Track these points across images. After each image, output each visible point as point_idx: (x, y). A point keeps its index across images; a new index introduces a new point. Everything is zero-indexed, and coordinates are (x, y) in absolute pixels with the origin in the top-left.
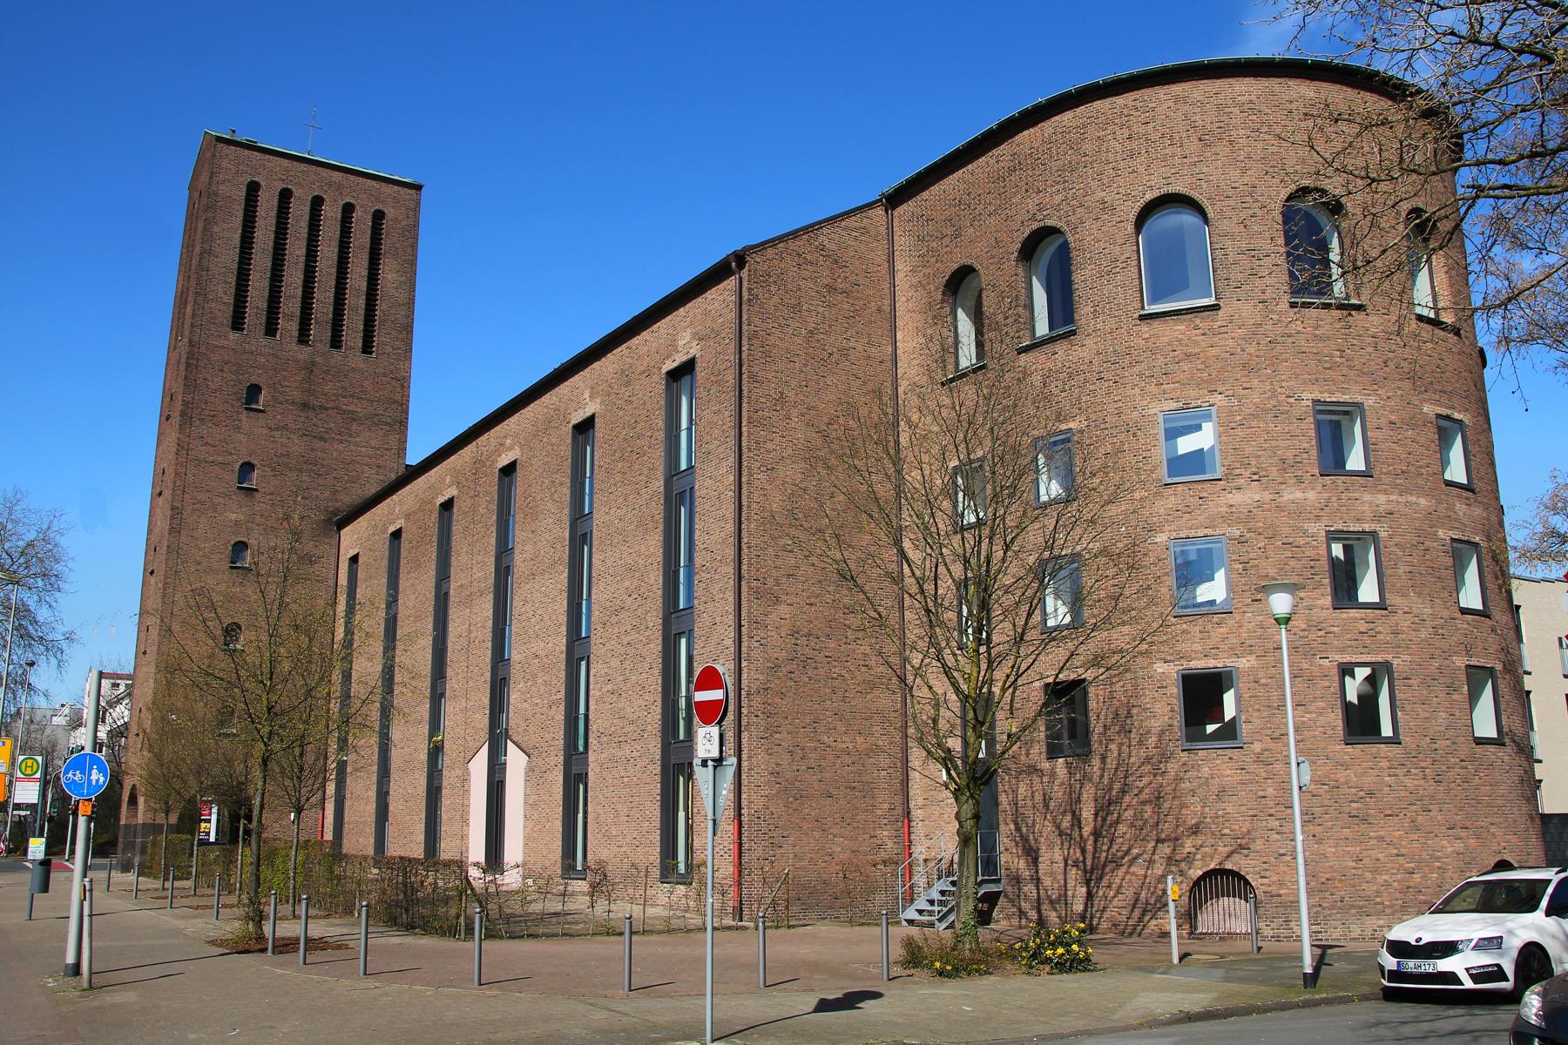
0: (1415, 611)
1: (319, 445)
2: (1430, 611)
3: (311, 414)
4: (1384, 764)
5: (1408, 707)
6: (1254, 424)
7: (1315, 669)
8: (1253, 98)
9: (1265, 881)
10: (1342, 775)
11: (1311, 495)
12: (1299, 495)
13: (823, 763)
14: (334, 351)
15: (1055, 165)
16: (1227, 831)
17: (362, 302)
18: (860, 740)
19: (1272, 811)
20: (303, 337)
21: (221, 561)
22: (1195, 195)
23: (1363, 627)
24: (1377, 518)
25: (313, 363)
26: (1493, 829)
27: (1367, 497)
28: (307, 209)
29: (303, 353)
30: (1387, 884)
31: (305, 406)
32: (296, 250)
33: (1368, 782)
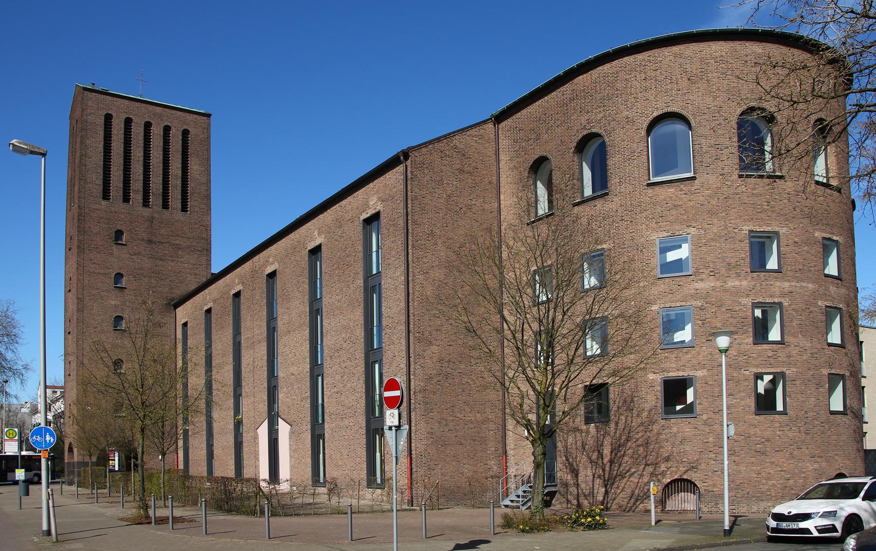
0: (801, 345)
1: (160, 263)
2: (809, 345)
3: (154, 246)
4: (777, 425)
5: (793, 396)
8: (723, 53)
10: (752, 431)
12: (737, 283)
14: (165, 211)
15: (598, 96)
17: (179, 182)
18: (478, 415)
20: (146, 203)
21: (108, 326)
22: (684, 113)
23: (770, 354)
24: (783, 295)
25: (153, 218)
27: (778, 284)
28: (142, 129)
29: (146, 212)
30: (774, 485)
31: (150, 242)
32: (137, 153)
33: (768, 434)
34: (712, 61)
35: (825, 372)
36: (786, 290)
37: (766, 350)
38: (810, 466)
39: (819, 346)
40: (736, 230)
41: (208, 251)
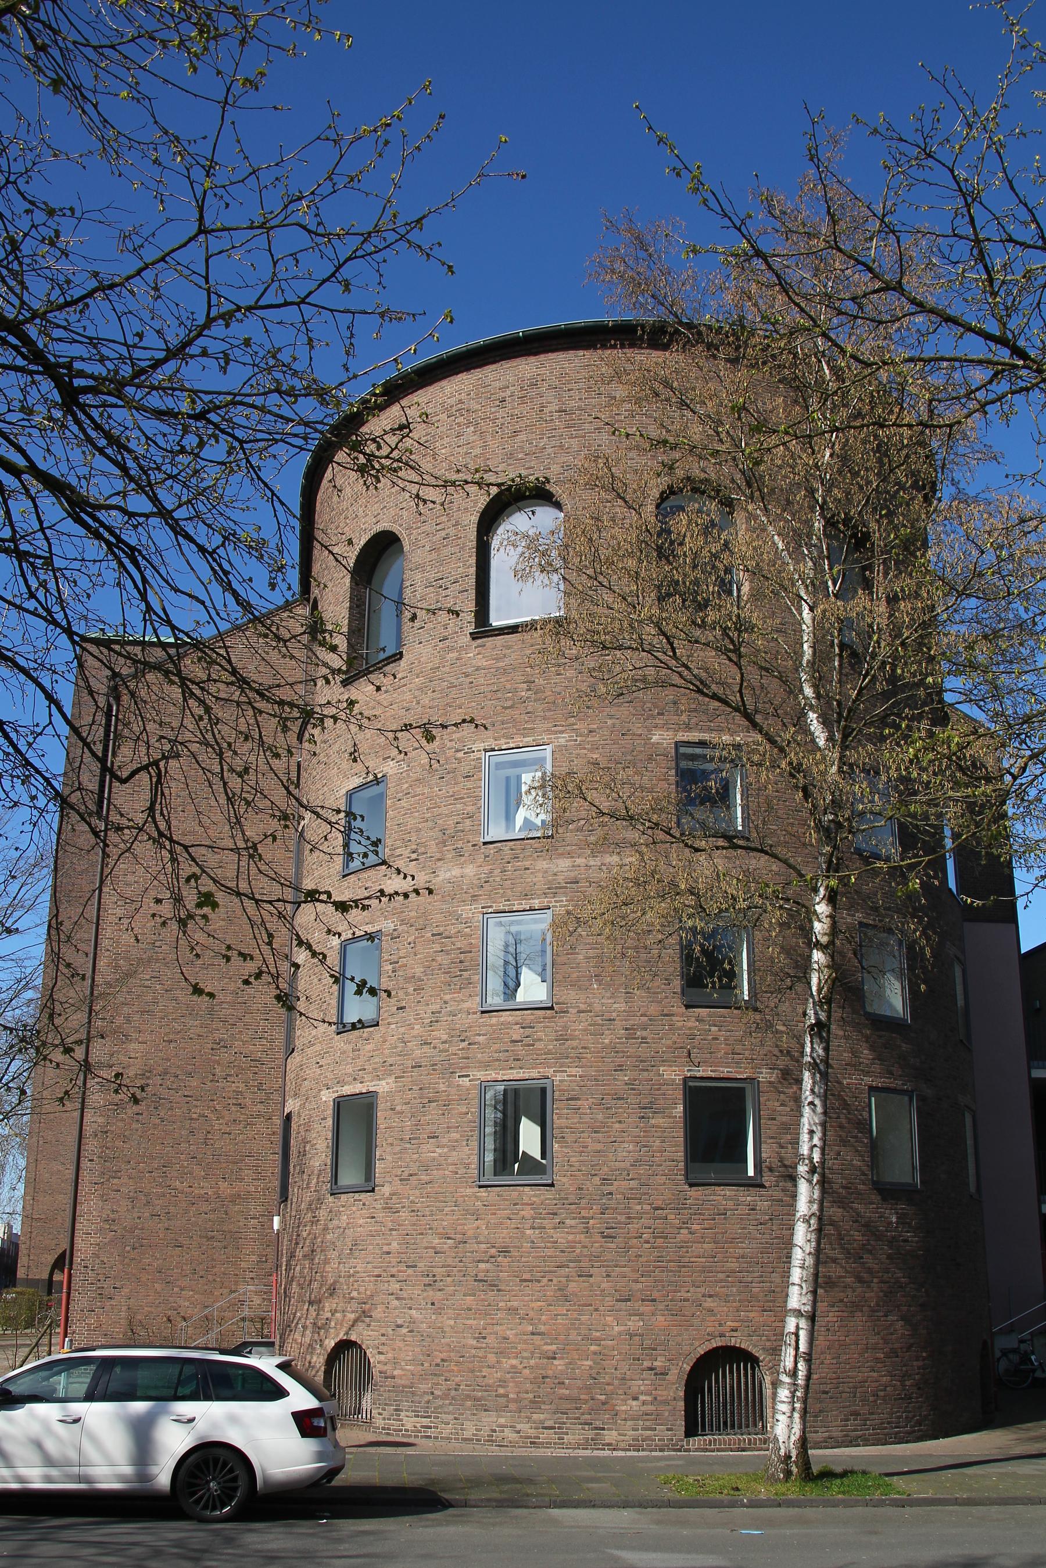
0: (597, 1007)
2: (621, 1006)
4: (527, 1212)
5: (570, 1138)
6: (418, 790)
7: (453, 1091)
8: (463, 396)
9: (382, 1357)
10: (470, 1226)
11: (470, 870)
12: (456, 872)
13: (172, 1209)
16: (354, 1294)
18: (223, 1185)
19: (394, 1271)
23: (517, 1033)
26: (709, 1303)
27: (542, 864)
30: (514, 1370)
33: (502, 1236)
34: (444, 417)
35: (674, 1074)
36: (560, 878)
37: (507, 1025)
38: (616, 1326)
39: (653, 1009)
40: (460, 755)
41: (1013, 919)
